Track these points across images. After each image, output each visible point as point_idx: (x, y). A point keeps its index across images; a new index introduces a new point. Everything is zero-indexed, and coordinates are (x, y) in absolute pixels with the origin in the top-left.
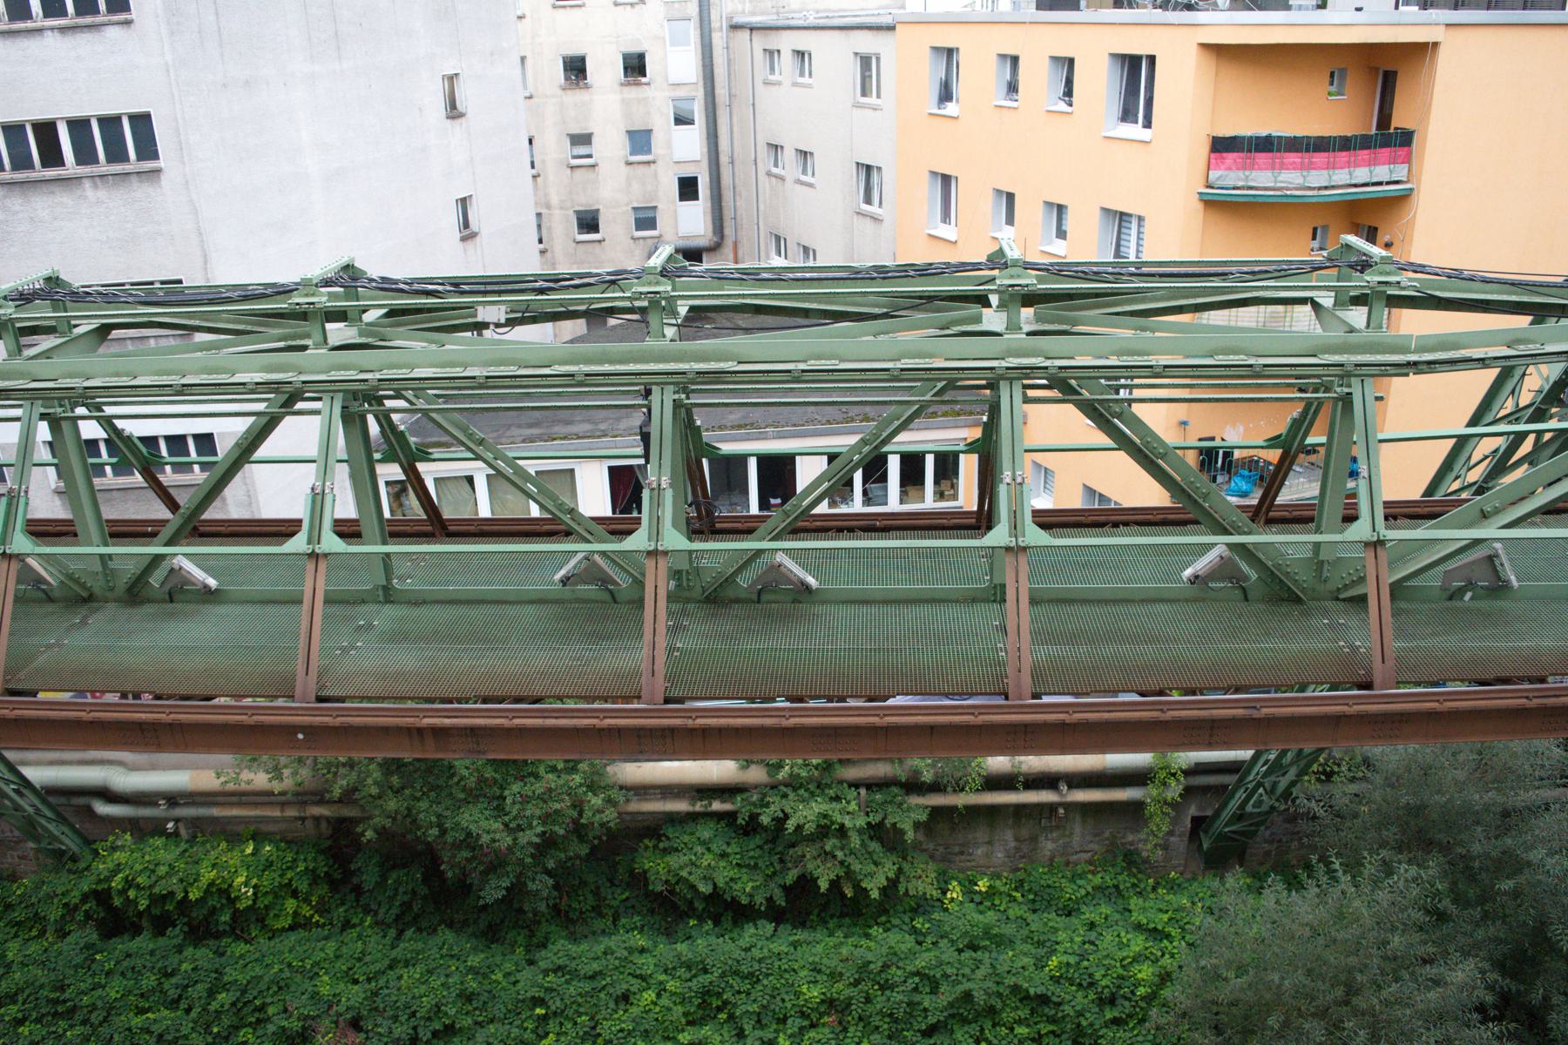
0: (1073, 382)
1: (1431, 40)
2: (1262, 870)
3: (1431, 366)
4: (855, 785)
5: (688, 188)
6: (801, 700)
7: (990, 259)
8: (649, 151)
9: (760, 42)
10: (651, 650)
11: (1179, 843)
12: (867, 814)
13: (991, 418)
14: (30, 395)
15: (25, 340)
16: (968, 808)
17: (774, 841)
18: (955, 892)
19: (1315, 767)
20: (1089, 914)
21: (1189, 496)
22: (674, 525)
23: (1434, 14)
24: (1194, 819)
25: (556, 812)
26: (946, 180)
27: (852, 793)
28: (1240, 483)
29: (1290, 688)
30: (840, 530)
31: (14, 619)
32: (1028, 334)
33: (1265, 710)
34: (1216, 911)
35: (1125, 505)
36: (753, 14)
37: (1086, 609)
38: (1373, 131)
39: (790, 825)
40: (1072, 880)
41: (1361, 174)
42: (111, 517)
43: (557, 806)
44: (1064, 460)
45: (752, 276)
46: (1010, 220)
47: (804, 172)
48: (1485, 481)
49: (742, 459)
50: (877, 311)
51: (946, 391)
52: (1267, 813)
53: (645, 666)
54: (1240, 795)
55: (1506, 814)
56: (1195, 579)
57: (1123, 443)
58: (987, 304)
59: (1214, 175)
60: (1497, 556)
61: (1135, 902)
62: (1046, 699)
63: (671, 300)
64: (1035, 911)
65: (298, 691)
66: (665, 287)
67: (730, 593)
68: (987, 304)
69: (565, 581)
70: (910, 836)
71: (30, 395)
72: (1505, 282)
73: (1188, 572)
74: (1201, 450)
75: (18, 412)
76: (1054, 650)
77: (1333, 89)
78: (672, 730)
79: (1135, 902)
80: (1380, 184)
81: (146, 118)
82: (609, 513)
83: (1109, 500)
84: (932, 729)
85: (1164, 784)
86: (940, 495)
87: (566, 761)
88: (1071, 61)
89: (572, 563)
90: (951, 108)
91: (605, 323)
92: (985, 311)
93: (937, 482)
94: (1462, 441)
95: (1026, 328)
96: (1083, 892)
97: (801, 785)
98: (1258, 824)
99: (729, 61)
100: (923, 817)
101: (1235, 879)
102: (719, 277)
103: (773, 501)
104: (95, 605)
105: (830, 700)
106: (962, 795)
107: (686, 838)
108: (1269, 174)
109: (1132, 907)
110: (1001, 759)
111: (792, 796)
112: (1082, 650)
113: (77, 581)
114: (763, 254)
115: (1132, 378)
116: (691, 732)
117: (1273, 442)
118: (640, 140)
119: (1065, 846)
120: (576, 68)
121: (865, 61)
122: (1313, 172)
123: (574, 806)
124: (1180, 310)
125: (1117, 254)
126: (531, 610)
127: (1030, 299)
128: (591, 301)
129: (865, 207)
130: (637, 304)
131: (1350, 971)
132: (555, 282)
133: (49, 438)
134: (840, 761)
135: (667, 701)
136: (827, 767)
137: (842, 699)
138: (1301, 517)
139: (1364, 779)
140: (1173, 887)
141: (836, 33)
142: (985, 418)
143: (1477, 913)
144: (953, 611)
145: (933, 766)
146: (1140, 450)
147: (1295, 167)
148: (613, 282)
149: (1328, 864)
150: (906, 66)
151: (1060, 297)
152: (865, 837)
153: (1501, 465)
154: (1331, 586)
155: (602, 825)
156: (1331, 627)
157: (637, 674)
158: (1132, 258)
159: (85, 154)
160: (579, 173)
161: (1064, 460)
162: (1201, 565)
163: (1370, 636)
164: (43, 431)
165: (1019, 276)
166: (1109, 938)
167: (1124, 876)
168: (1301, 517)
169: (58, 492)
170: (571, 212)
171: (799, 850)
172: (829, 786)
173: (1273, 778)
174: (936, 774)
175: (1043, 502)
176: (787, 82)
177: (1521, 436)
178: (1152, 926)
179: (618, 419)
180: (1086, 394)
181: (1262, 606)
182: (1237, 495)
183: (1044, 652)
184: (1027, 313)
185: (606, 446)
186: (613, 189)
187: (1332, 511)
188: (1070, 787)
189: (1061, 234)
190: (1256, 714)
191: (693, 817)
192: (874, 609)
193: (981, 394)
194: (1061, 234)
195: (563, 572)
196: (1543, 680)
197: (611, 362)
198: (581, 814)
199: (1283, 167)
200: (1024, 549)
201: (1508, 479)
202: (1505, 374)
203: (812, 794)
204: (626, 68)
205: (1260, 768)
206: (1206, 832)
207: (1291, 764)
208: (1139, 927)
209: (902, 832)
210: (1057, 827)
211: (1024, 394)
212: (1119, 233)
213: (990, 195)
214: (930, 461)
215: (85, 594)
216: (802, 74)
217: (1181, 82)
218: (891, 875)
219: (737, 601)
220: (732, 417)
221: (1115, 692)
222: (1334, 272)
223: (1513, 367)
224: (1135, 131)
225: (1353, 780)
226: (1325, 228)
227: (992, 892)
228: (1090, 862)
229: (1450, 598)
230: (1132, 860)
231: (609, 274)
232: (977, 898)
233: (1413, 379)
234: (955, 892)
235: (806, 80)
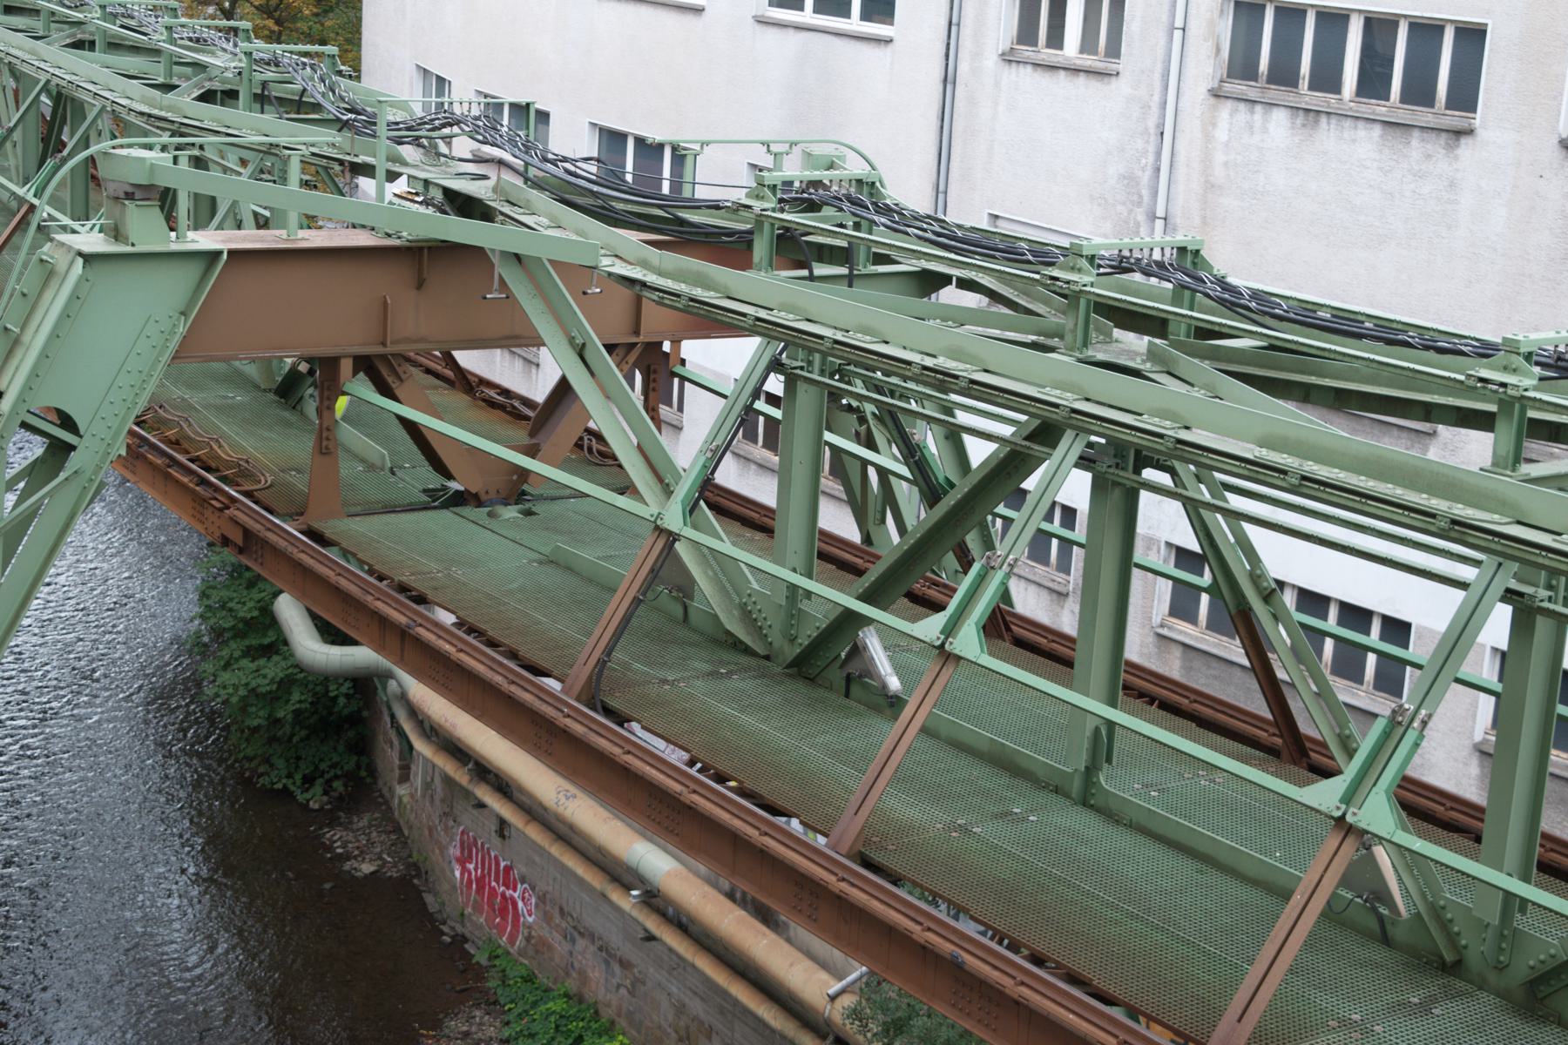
14: (1500, 546)
15: (1533, 447)
31: (1310, 944)
42: (1557, 833)
65: (835, 832)
71: (1500, 546)
75: (1467, 573)
81: (1472, 37)
104: (1460, 984)
113: (1445, 925)
133: (1504, 646)
137: (896, 880)
159: (1373, 82)
164: (1498, 626)
169: (1481, 751)
215: (1449, 957)
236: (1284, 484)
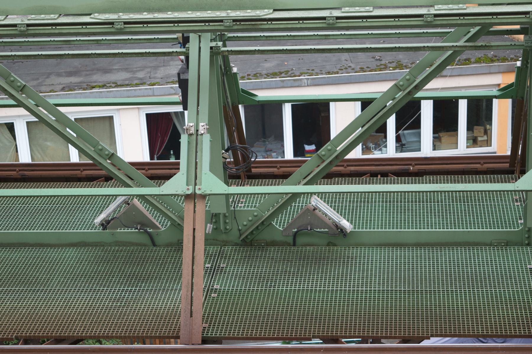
30: (374, 175)
49: (276, 106)
53: (184, 307)
67: (266, 235)
69: (105, 225)
73: (98, 220)
82: (146, 158)
86: (473, 141)
89: (112, 207)
93: (470, 128)
103: (307, 148)
126: (71, 252)
135: (205, 341)
142: (519, 64)
144: (486, 255)
179: (156, 68)
192: (408, 253)
195: (103, 216)
220: (267, 65)
236: (113, 30)
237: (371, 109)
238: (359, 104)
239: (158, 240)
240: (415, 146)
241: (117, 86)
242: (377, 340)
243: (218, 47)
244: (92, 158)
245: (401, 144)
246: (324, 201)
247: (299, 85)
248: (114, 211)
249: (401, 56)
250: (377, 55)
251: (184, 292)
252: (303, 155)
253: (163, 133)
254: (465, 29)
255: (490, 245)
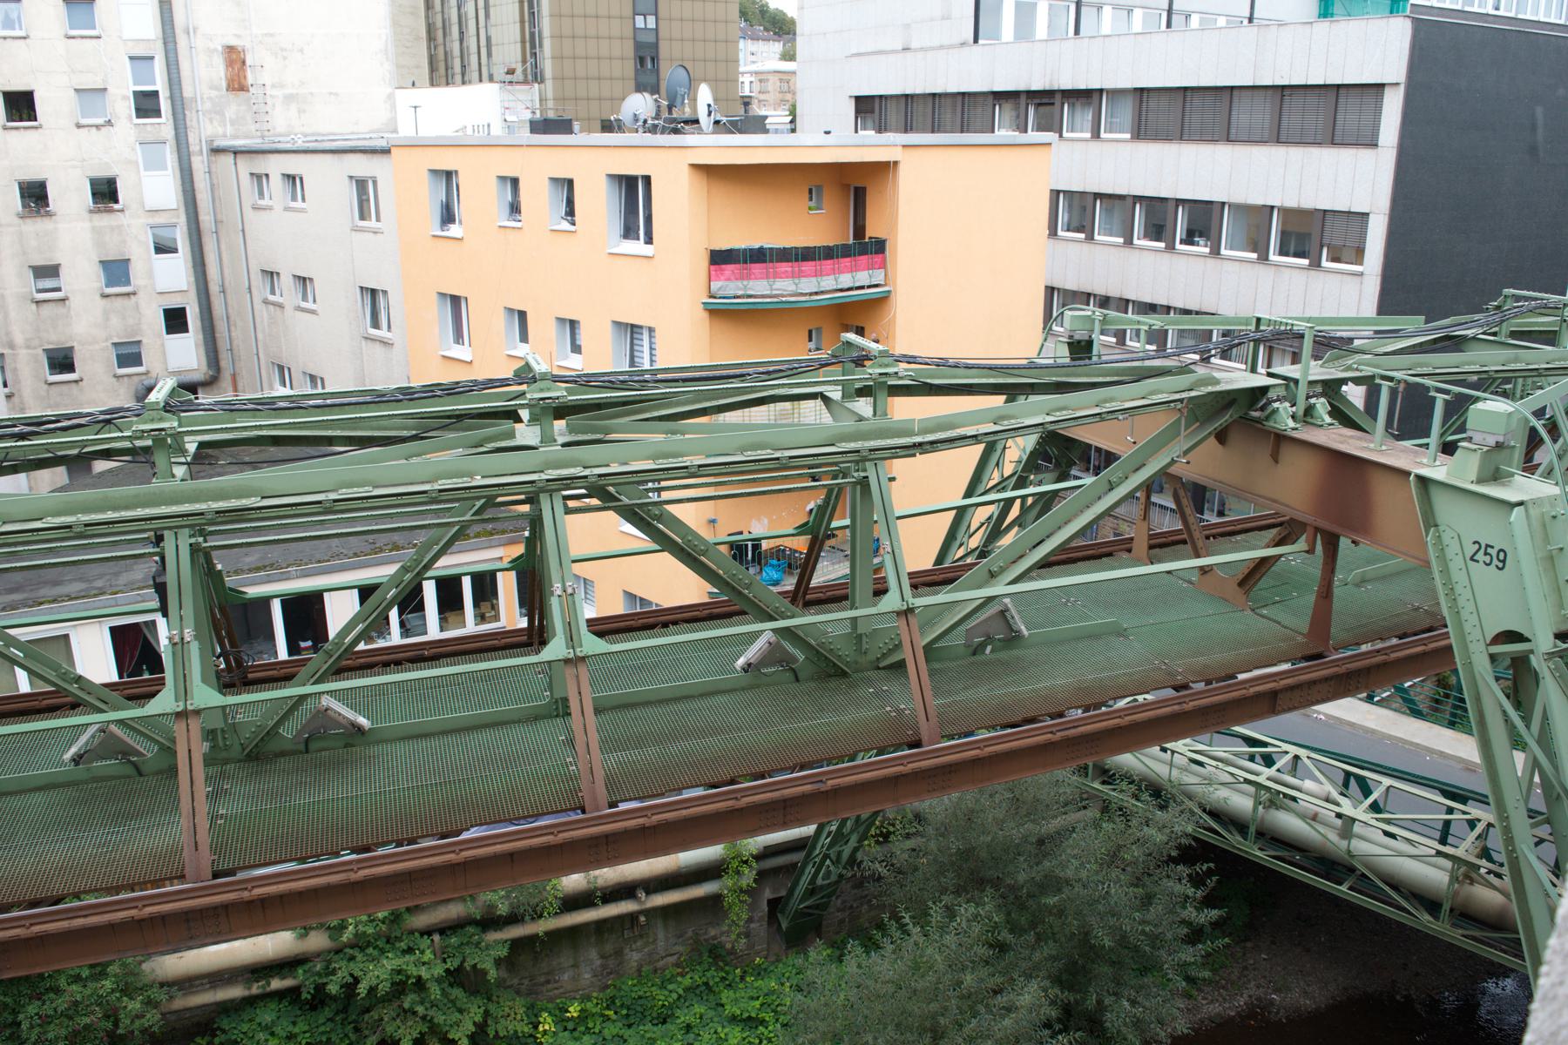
0: (611, 489)
1: (892, 159)
2: (839, 938)
3: (934, 446)
4: (427, 932)
5: (175, 320)
6: (367, 849)
7: (517, 373)
8: (128, 283)
9: (245, 166)
10: (190, 822)
11: (760, 928)
12: (444, 961)
13: (533, 532)
16: (547, 933)
17: (345, 1010)
18: (547, 1024)
19: (873, 832)
20: (684, 1017)
21: (734, 588)
22: (204, 680)
23: (891, 137)
24: (770, 902)
25: (86, 1027)
26: (456, 301)
27: (426, 941)
28: (770, 573)
29: (841, 759)
30: (386, 664)
32: (563, 445)
33: (830, 783)
34: (804, 987)
35: (666, 605)
36: (235, 137)
37: (650, 711)
38: (851, 241)
39: (362, 989)
40: (663, 987)
41: (846, 280)
43: (87, 1020)
44: (610, 566)
45: (268, 406)
46: (524, 338)
47: (305, 298)
48: (985, 545)
49: (265, 602)
50: (405, 433)
51: (483, 510)
52: (837, 882)
53: (185, 839)
54: (810, 870)
55: (1041, 842)
56: (748, 667)
57: (666, 544)
58: (519, 420)
59: (715, 285)
60: (1007, 610)
61: (726, 996)
62: (623, 806)
63: (178, 436)
64: (630, 1026)
65: (188, 871)
66: (171, 423)
67: (274, 746)
68: (519, 420)
69: (77, 759)
70: (493, 974)
72: (991, 368)
73: (741, 661)
74: (732, 545)
76: (633, 755)
77: (812, 204)
78: (226, 907)
79: (726, 996)
80: (862, 288)
82: (115, 678)
83: (650, 603)
84: (511, 856)
85: (738, 872)
86: (481, 618)
87: (92, 966)
88: (570, 182)
89: (84, 739)
90: (454, 230)
91: (89, 469)
92: (517, 426)
93: (476, 605)
94: (961, 512)
95: (561, 440)
96: (675, 996)
97: (369, 944)
98: (829, 896)
99: (212, 185)
100: (504, 952)
101: (818, 952)
102: (231, 409)
103: (303, 644)
105: (400, 844)
106: (541, 922)
107: (245, 1027)
108: (765, 282)
109: (724, 1000)
110: (575, 877)
111: (360, 957)
112: (652, 751)
114: (265, 385)
115: (659, 481)
116: (249, 905)
117: (802, 529)
118: (116, 271)
119: (650, 954)
120: (35, 195)
121: (361, 184)
122: (804, 280)
123: (107, 1017)
124: (703, 412)
125: (632, 364)
126: (38, 798)
127: (561, 411)
128: (85, 443)
129: (373, 331)
130: (139, 443)
131: (934, 1016)
132: (38, 425)
134: (408, 909)
135: (216, 875)
136: (395, 918)
138: (836, 596)
139: (917, 834)
140: (760, 973)
141: (329, 157)
142: (527, 534)
143: (1031, 937)
144: (517, 732)
145: (507, 897)
146: (682, 549)
147: (786, 275)
148: (108, 422)
149: (898, 919)
150: (405, 190)
151: (590, 407)
152: (445, 985)
153: (996, 530)
154: (871, 657)
155: (144, 1031)
156: (876, 694)
157: (176, 851)
158: (647, 366)
160: (46, 310)
161: (610, 566)
162: (752, 653)
163: (913, 698)
165: (549, 389)
166: (707, 1036)
167: (712, 972)
168: (836, 596)
170: (40, 351)
171: (375, 1015)
172: (399, 939)
173: (837, 848)
174: (511, 904)
175: (590, 612)
176: (278, 207)
177: (1009, 503)
178: (745, 1015)
179: (117, 574)
180: (626, 501)
181: (813, 685)
182: (777, 583)
183: (614, 758)
184: (560, 424)
185: (103, 603)
186: (88, 323)
187: (863, 588)
188: (648, 893)
189: (576, 349)
190: (823, 787)
191: (250, 1002)
192: (434, 743)
193: (522, 512)
194: (576, 349)
195: (74, 750)
196: (1061, 715)
197: (115, 509)
198: (116, 1024)
199: (777, 276)
200: (583, 659)
201: (1007, 540)
202: (990, 449)
203: (382, 951)
204: (94, 194)
205: (825, 841)
206: (782, 912)
207: (852, 831)
208: (734, 1019)
209: (484, 973)
210: (641, 936)
211: (565, 506)
212: (632, 344)
213: (502, 314)
214: (467, 583)
216: (294, 199)
217: (676, 199)
218: (478, 1018)
219: (283, 754)
220: (248, 560)
221: (679, 790)
222: (838, 368)
223: (995, 442)
224: (637, 247)
225: (908, 836)
226: (819, 330)
227: (584, 1016)
228: (677, 965)
229: (974, 654)
230: (717, 955)
231: (103, 413)
232: (570, 1025)
233: (920, 459)
234: (547, 1024)
235: (299, 204)
237: (373, 600)
238: (356, 591)
239: (144, 769)
240: (421, 629)
241: (72, 599)
242: (412, 841)
243: (198, 544)
244: (55, 685)
245: (405, 630)
246: (335, 699)
247: (287, 577)
248: (87, 743)
249: (396, 537)
250: (370, 538)
251: (184, 822)
252: (299, 653)
253: (134, 648)
254: (469, 503)
255: (519, 721)
